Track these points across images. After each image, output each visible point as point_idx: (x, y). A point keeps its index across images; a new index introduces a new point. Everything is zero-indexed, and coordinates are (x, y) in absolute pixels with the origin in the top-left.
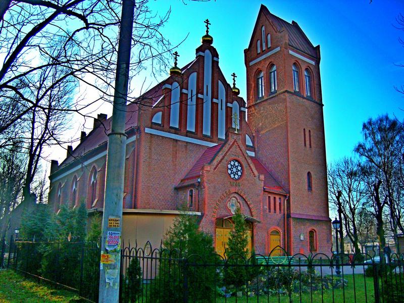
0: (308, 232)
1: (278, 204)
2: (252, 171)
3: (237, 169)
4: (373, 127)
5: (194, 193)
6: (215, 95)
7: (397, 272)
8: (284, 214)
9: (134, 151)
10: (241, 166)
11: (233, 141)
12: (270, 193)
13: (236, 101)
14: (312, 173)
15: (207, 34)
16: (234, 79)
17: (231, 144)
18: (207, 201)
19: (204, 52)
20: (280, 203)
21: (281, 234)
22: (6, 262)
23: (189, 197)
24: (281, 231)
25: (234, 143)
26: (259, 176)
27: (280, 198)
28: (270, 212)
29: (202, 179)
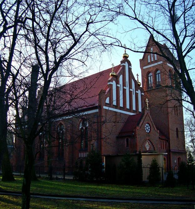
6: (130, 87)
10: (150, 126)
11: (146, 113)
12: (161, 139)
14: (178, 128)
16: (137, 77)
18: (138, 144)
20: (165, 144)
22: (146, 173)
23: (126, 142)
28: (161, 149)
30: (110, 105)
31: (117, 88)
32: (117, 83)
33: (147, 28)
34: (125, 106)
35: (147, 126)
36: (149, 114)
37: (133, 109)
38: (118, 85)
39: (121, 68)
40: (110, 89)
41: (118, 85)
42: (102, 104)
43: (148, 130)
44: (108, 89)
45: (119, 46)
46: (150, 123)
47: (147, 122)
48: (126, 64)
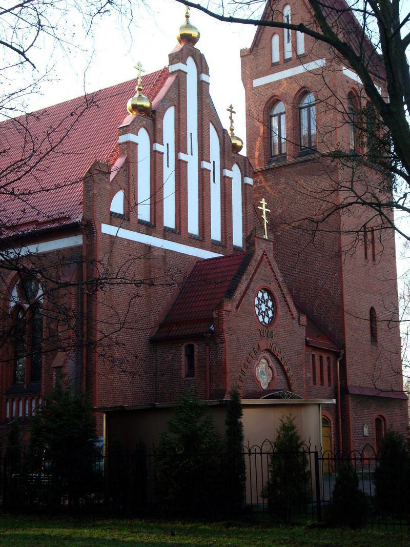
0: (374, 420)
1: (325, 368)
2: (289, 308)
3: (266, 306)
5: (196, 350)
6: (203, 155)
7: (253, 503)
8: (336, 387)
10: (273, 300)
13: (144, 127)
15: (188, 23)
16: (231, 118)
17: (259, 259)
19: (185, 63)
20: (329, 367)
21: (332, 426)
23: (184, 359)
24: (331, 418)
25: (262, 258)
26: (299, 317)
27: (328, 358)
28: (315, 384)
30: (127, 219)
31: (156, 158)
32: (155, 136)
35: (262, 300)
36: (271, 255)
38: (158, 147)
39: (170, 80)
43: (265, 314)
44: (119, 162)
46: (273, 287)
48: (190, 67)
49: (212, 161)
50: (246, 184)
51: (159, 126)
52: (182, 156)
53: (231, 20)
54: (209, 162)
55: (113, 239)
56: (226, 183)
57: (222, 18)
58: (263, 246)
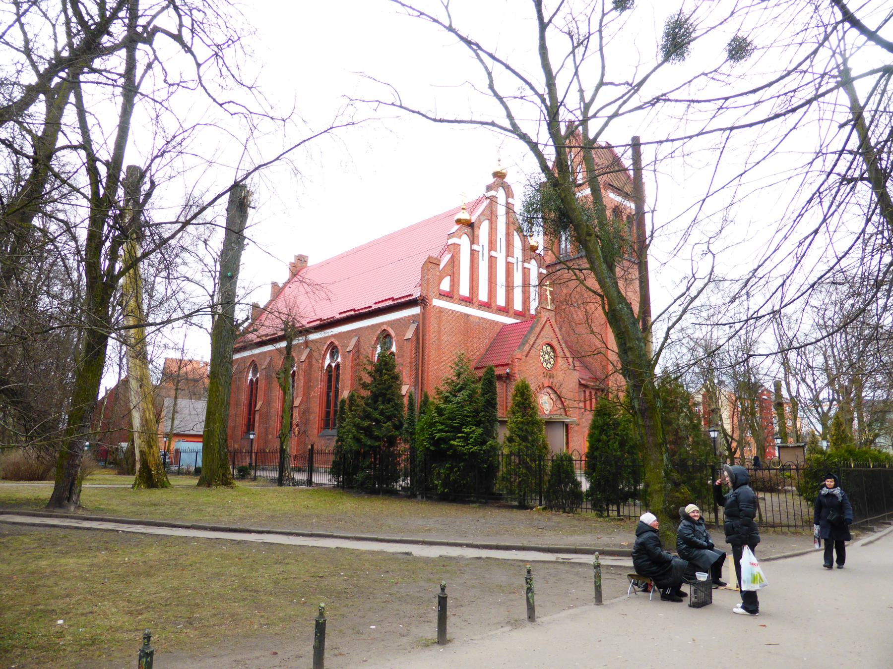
4: (153, 278)
6: (509, 252)
9: (418, 326)
25: (546, 322)
29: (512, 369)
30: (448, 296)
31: (473, 254)
32: (473, 240)
33: (477, 55)
34: (455, 288)
35: (545, 353)
36: (553, 321)
37: (515, 308)
38: (475, 247)
39: (486, 202)
40: (453, 257)
41: (510, 259)
42: (430, 294)
43: (547, 361)
44: (446, 258)
45: (393, 104)
46: (555, 343)
47: (545, 340)
48: (501, 195)
49: (515, 256)
50: (541, 273)
51: (476, 233)
52: (493, 253)
53: (441, 121)
54: (513, 257)
55: (441, 310)
56: (526, 273)
57: (435, 120)
58: (547, 314)
